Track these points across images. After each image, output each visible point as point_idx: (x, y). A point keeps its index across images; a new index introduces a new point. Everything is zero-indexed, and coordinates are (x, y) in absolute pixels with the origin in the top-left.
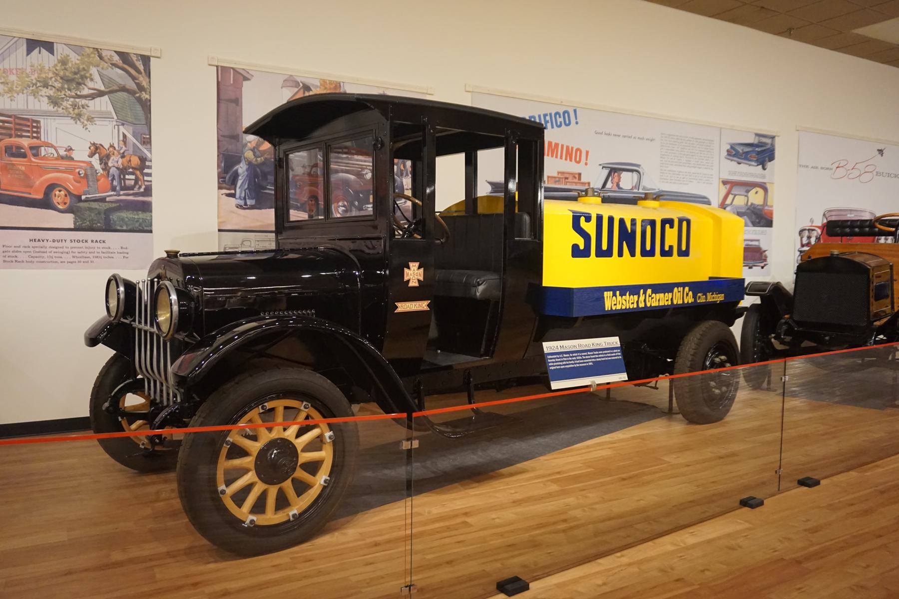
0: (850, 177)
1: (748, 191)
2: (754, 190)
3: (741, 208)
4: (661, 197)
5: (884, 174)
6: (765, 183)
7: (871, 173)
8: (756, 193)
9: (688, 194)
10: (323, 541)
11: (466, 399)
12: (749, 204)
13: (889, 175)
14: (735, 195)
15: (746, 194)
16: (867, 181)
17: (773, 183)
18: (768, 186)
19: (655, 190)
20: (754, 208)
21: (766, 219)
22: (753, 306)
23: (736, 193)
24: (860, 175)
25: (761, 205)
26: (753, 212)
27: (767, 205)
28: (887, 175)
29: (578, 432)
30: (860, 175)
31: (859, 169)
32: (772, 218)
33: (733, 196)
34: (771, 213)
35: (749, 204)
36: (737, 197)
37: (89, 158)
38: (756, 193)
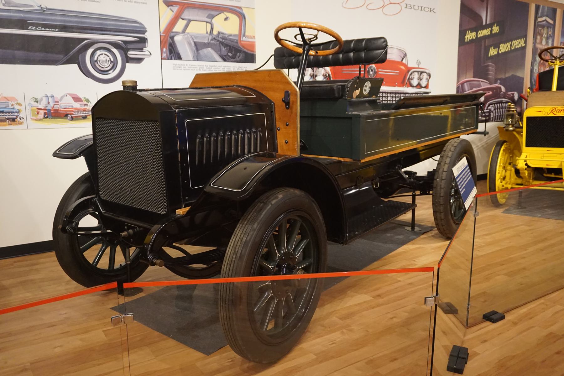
0: (369, 7)
1: (212, 17)
2: (222, 16)
3: (203, 37)
4: (212, 30)
5: (416, 7)
6: (240, 8)
7: (398, 5)
8: (226, 19)
9: (106, 15)
10: (144, 274)
11: (465, 77)
12: (215, 32)
13: (422, 9)
14: (189, 21)
15: (209, 20)
16: (362, 5)
17: (254, 8)
18: (245, 11)
19: (31, 6)
20: (223, 38)
21: (246, 53)
22: (123, 232)
23: (191, 18)
24: (383, 6)
25: (235, 35)
26: (221, 43)
27: (244, 35)
28: (420, 8)
29: (468, 94)
30: (383, 6)
31: (401, 6)
32: (254, 51)
33: (185, 22)
34: (253, 45)
35: (215, 32)
36: (192, 22)
37: (3, 6)
38: (226, 19)
